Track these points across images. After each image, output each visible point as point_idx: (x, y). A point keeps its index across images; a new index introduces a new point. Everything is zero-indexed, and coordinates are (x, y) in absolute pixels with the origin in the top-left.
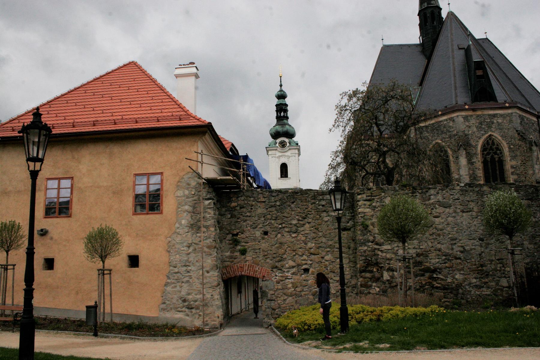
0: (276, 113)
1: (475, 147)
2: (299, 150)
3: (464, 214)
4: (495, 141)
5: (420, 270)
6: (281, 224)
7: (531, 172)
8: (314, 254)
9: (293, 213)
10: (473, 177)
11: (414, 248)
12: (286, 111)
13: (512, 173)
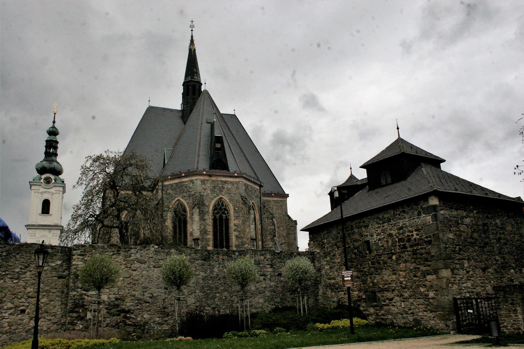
0: (45, 148)
1: (208, 207)
2: (64, 188)
3: (155, 269)
4: (224, 203)
5: (117, 311)
6: (5, 271)
7: (248, 230)
8: (32, 298)
9: (17, 262)
10: (204, 232)
11: (114, 294)
12: (56, 148)
13: (235, 230)
